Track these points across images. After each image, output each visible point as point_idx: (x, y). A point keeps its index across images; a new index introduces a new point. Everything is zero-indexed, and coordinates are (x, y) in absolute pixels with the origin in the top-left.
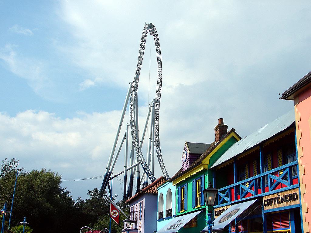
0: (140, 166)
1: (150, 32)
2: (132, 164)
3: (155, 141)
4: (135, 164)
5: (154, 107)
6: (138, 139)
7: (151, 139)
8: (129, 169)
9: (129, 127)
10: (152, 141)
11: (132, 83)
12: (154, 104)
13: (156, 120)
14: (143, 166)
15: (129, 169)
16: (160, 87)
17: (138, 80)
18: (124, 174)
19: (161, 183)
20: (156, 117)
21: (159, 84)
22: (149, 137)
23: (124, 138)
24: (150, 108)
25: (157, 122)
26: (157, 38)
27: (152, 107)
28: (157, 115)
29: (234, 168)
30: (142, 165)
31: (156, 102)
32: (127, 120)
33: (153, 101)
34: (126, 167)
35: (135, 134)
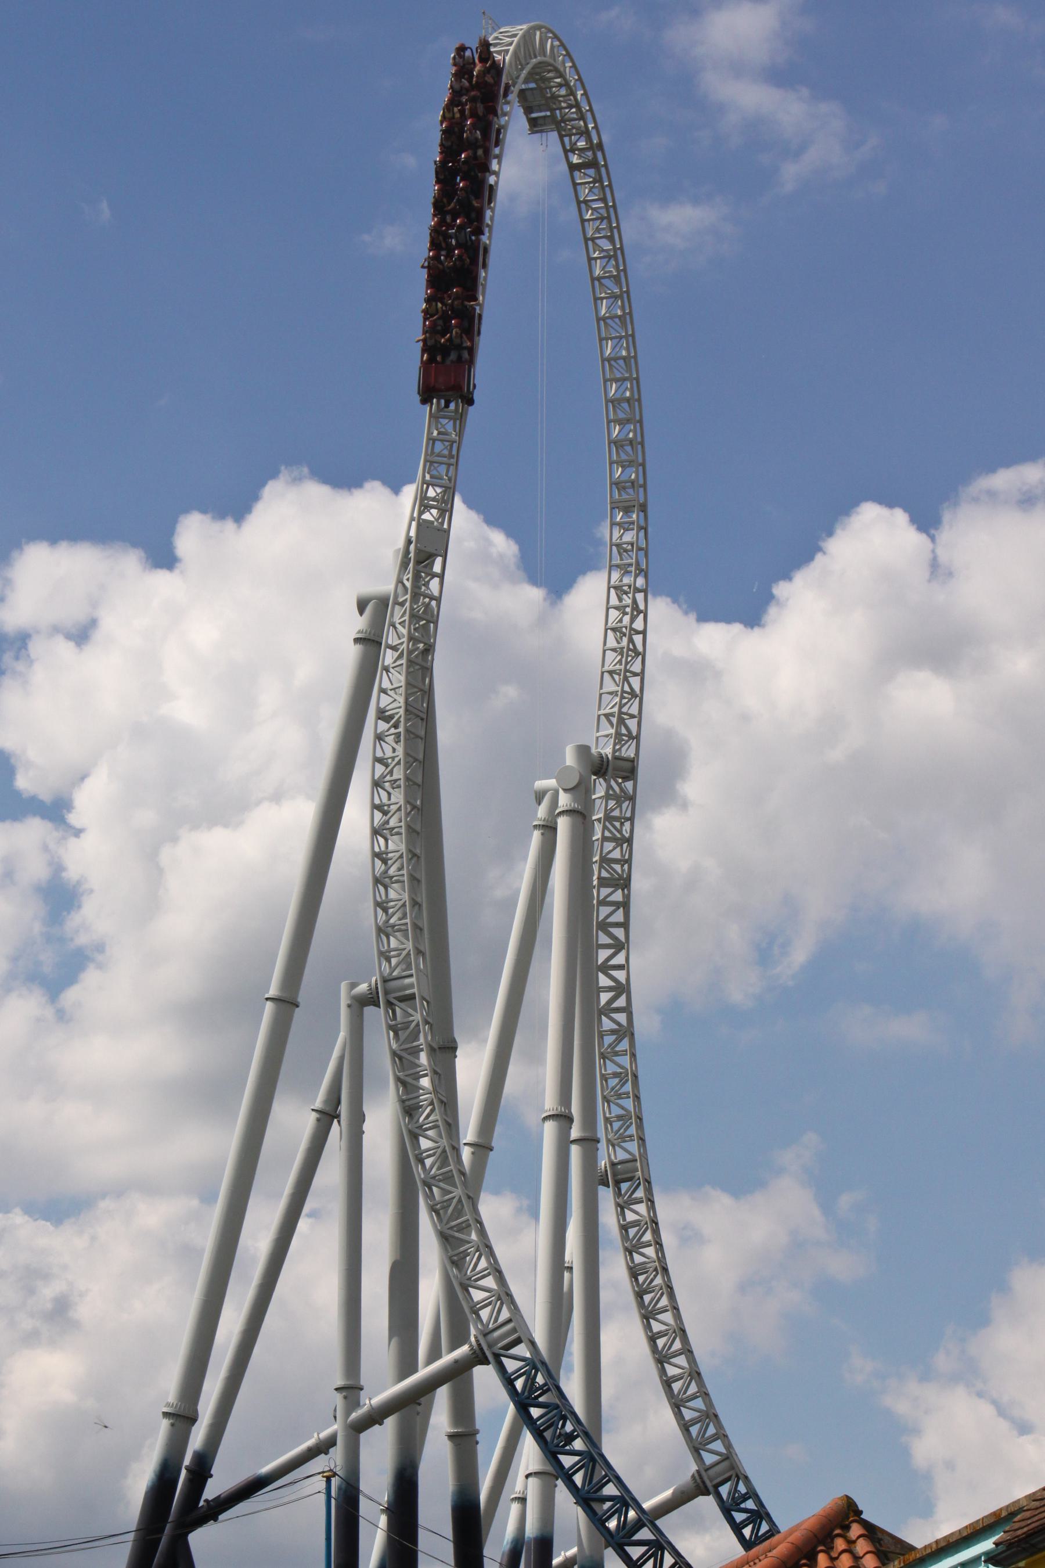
0: (484, 1377)
1: (528, 110)
2: (407, 1364)
3: (601, 1133)
4: (375, 1398)
5: (581, 815)
6: (451, 1126)
7: (564, 1118)
8: (375, 1418)
9: (376, 1017)
10: (575, 1133)
11: (383, 603)
12: (581, 789)
13: (604, 939)
14: (508, 1381)
15: (375, 1418)
16: (638, 624)
17: (437, 568)
18: (336, 1459)
19: (851, 1542)
20: (604, 911)
21: (627, 600)
22: (550, 1103)
23: (327, 1116)
24: (549, 829)
25: (619, 959)
26: (593, 164)
27: (563, 824)
28: (618, 896)
29: (174, 1505)
30: (501, 1369)
31: (600, 768)
32: (501, 136)
33: (570, 759)
34: (351, 1390)
35: (425, 1082)
